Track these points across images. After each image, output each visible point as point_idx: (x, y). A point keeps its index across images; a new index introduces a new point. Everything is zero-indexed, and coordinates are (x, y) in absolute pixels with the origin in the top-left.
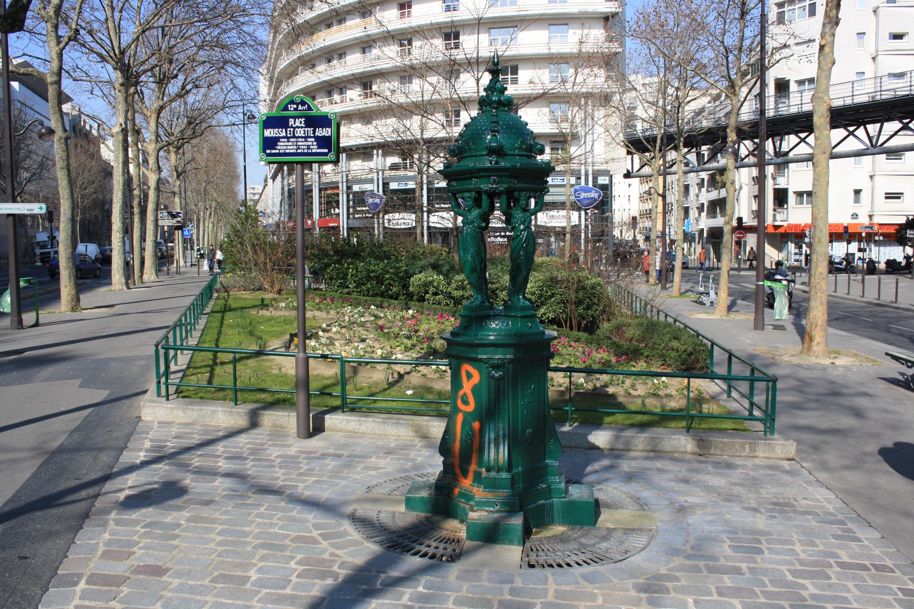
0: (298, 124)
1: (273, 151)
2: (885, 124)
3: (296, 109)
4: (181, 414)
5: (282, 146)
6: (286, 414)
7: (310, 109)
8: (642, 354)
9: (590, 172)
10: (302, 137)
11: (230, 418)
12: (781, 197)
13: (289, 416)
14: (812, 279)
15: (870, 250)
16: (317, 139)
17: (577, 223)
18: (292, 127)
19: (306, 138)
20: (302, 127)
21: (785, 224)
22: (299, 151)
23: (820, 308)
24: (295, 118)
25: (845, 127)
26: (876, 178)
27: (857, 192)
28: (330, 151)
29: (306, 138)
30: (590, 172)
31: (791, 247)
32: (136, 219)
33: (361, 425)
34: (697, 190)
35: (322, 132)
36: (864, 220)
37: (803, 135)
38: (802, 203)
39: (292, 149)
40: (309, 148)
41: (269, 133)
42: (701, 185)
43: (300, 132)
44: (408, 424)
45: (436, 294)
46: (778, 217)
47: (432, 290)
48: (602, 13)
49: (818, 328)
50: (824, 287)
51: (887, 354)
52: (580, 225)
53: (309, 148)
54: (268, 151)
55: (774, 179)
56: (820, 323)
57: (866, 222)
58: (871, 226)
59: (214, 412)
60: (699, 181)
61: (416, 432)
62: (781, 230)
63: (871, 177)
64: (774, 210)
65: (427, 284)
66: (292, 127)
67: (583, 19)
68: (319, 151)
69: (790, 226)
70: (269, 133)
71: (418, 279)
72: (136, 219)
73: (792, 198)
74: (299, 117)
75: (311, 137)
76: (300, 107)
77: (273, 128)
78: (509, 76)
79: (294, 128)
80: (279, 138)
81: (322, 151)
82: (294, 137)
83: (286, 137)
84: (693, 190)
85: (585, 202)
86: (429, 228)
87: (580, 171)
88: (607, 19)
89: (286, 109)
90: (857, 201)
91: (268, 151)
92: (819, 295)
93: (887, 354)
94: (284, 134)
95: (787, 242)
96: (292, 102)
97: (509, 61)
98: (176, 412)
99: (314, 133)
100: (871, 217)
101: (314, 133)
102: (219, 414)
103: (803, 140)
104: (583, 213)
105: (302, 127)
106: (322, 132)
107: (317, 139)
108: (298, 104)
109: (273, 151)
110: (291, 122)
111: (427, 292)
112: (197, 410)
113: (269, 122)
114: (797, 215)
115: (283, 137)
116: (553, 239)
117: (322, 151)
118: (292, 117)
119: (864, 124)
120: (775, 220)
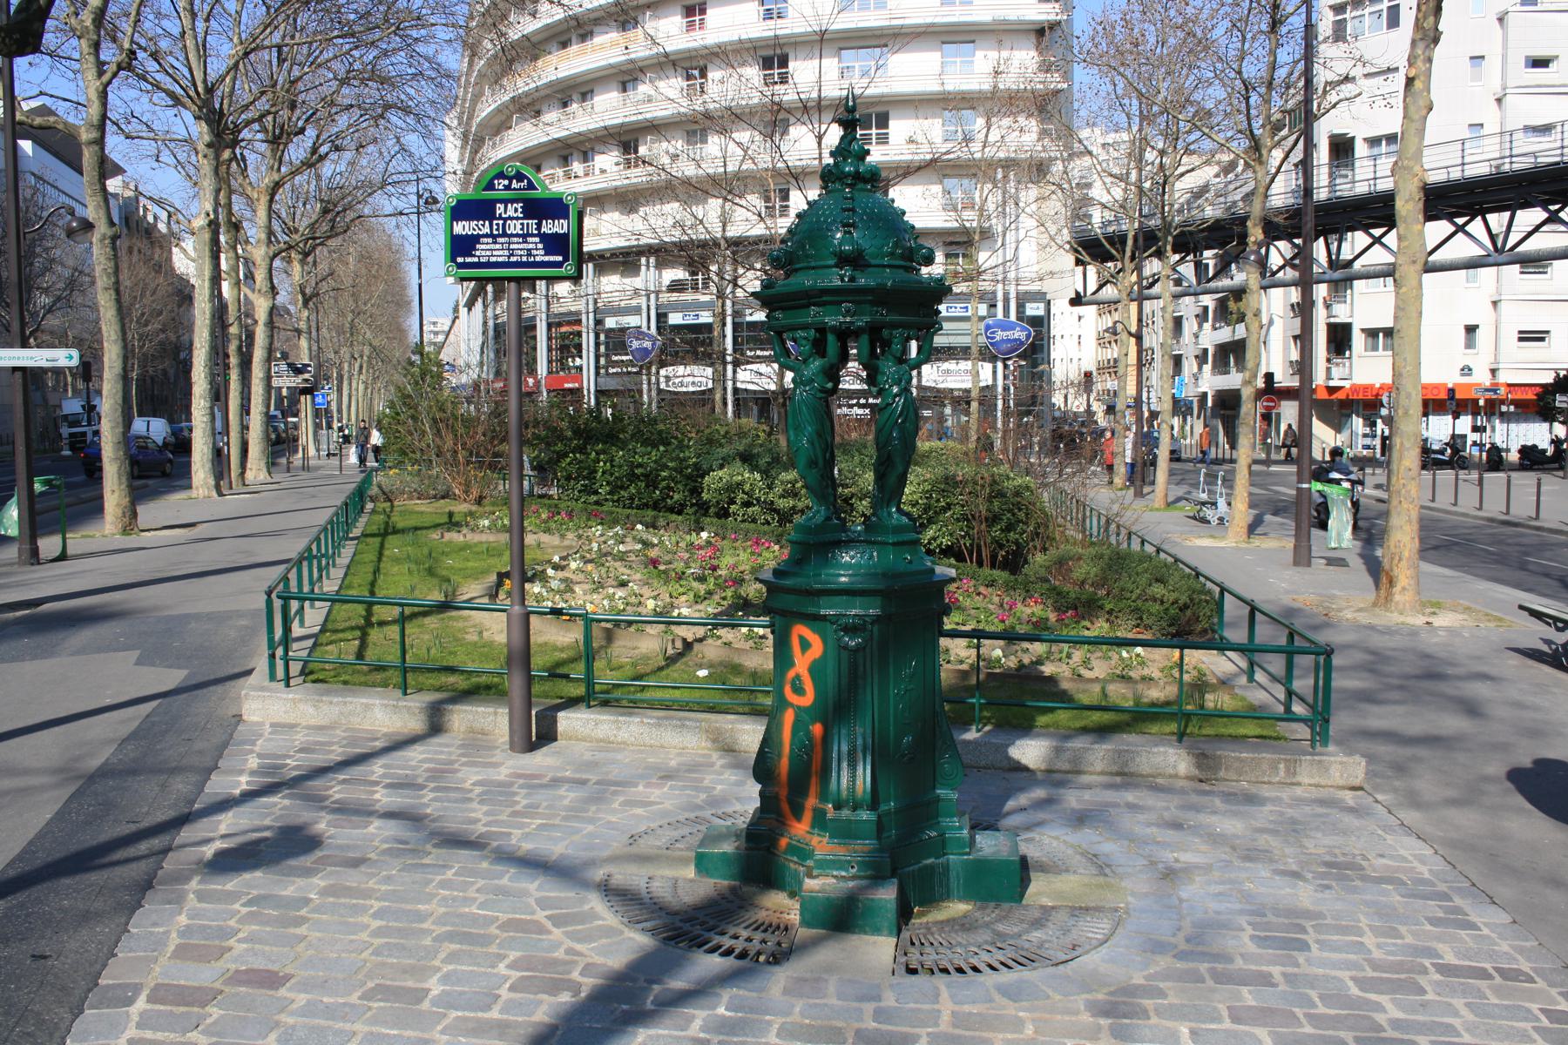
0: (510, 213)
1: (469, 260)
2: (1519, 212)
3: (508, 188)
4: (311, 710)
5: (483, 251)
6: (491, 710)
7: (531, 186)
8: (1101, 607)
9: (1013, 295)
10: (517, 235)
11: (394, 717)
12: (1340, 338)
13: (496, 713)
14: (1394, 479)
15: (1493, 429)
16: (545, 238)
17: (990, 382)
18: (500, 218)
19: (525, 236)
20: (517, 218)
21: (1347, 384)
22: (513, 259)
23: (1407, 528)
24: (506, 202)
25: (1450, 218)
26: (1503, 306)
27: (1471, 330)
28: (566, 259)
29: (525, 236)
30: (1013, 295)
31: (1358, 423)
32: (234, 376)
33: (619, 729)
34: (1196, 327)
35: (552, 227)
36: (1482, 377)
37: (1377, 232)
38: (1375, 348)
39: (500, 256)
40: (529, 255)
41: (461, 228)
42: (1202, 317)
43: (515, 227)
44: (700, 728)
45: (747, 504)
46: (1335, 372)
47: (740, 497)
48: (1033, 23)
49: (1404, 564)
50: (1413, 493)
51: (1521, 607)
52: (994, 386)
53: (529, 255)
54: (460, 260)
55: (1328, 307)
56: (1406, 554)
57: (1486, 380)
58: (1494, 389)
59: (367, 707)
60: (1199, 311)
61: (714, 741)
62: (1340, 395)
63: (1495, 303)
64: (1328, 360)
65: (733, 488)
66: (500, 218)
67: (999, 33)
68: (547, 258)
69: (1355, 388)
70: (461, 228)
71: (717, 479)
72: (234, 376)
73: (1358, 340)
74: (513, 201)
75: (533, 235)
76: (515, 184)
77: (469, 219)
78: (874, 131)
79: (505, 220)
80: (479, 236)
81: (552, 258)
82: (504, 234)
83: (491, 235)
84: (1190, 326)
85: (1004, 347)
86: (736, 390)
87: (994, 293)
88: (1041, 33)
89: (490, 186)
90: (1470, 344)
91: (460, 260)
92: (1405, 505)
93: (1521, 607)
94: (486, 230)
95: (1350, 416)
96: (501, 175)
97: (873, 104)
98: (301, 706)
99: (539, 228)
100: (1493, 372)
101: (539, 228)
102: (376, 710)
103: (1377, 240)
104: (1000, 365)
105: (517, 218)
106: (552, 227)
107: (545, 238)
108: (510, 179)
109: (469, 260)
110: (500, 209)
111: (732, 502)
112: (338, 703)
113: (462, 210)
114: (1367, 369)
115: (486, 236)
116: (948, 410)
117: (552, 258)
118: (500, 201)
119: (1483, 213)
120: (1329, 377)
